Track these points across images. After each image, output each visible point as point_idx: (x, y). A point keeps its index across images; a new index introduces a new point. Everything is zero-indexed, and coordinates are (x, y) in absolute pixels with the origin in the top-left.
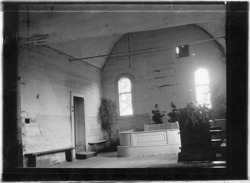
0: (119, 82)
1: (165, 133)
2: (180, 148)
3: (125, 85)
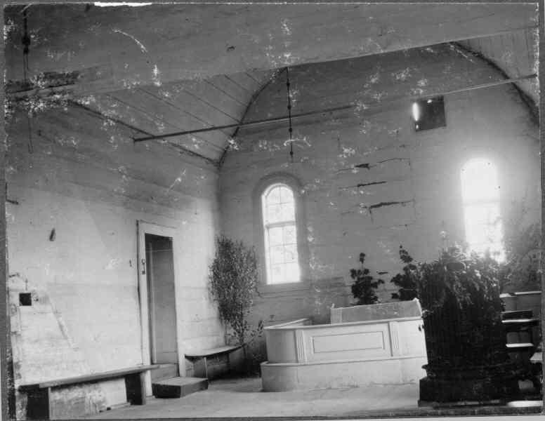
1: (384, 327)
2: (424, 367)
3: (279, 204)
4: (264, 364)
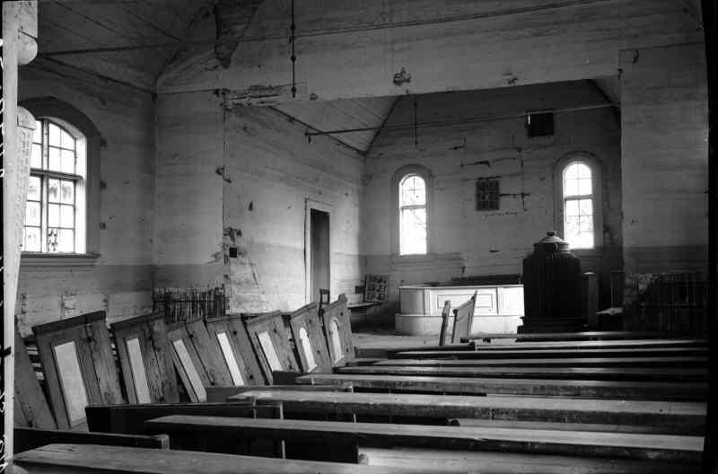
0: (400, 184)
1: (493, 291)
2: (522, 318)
3: (413, 189)
4: (397, 315)
